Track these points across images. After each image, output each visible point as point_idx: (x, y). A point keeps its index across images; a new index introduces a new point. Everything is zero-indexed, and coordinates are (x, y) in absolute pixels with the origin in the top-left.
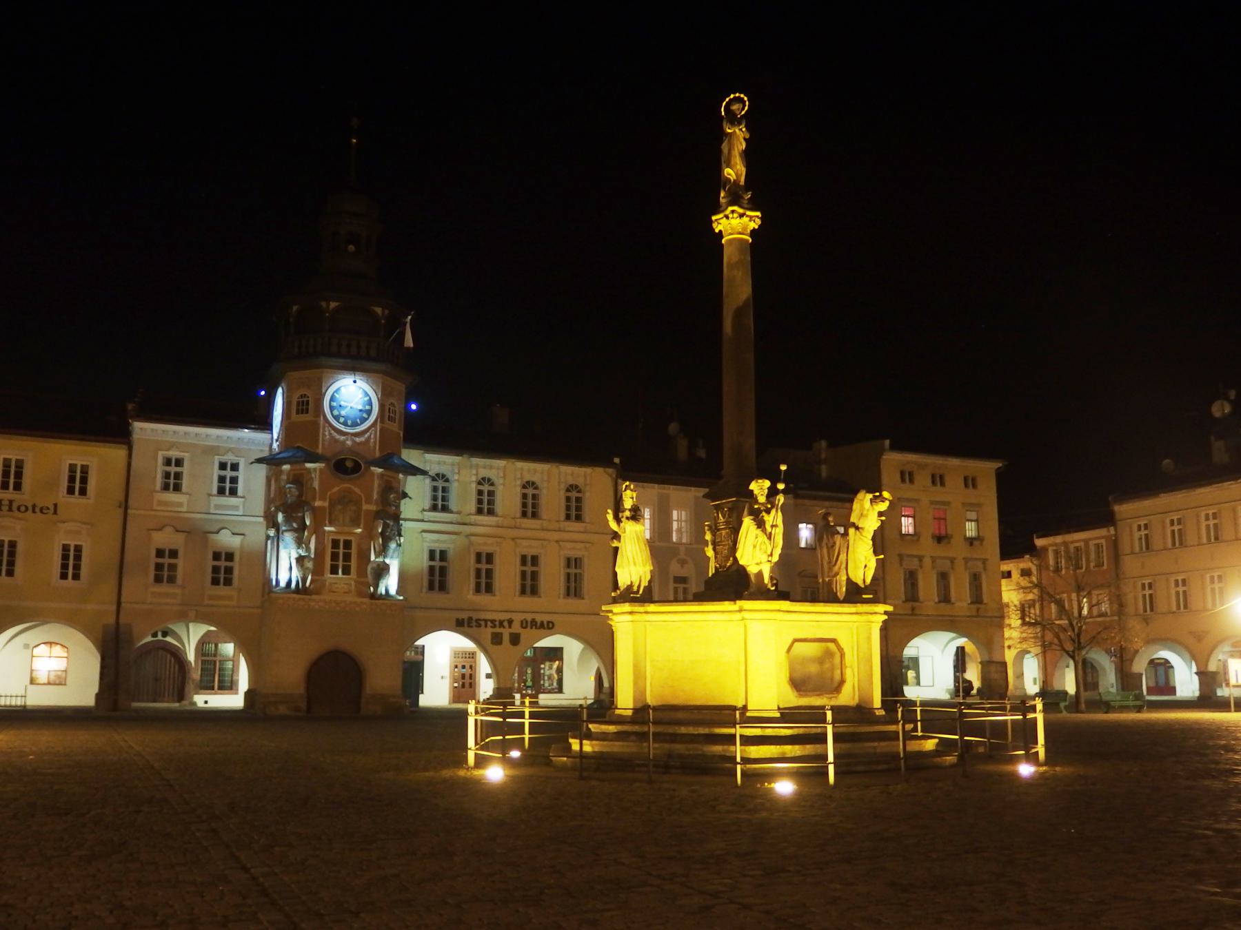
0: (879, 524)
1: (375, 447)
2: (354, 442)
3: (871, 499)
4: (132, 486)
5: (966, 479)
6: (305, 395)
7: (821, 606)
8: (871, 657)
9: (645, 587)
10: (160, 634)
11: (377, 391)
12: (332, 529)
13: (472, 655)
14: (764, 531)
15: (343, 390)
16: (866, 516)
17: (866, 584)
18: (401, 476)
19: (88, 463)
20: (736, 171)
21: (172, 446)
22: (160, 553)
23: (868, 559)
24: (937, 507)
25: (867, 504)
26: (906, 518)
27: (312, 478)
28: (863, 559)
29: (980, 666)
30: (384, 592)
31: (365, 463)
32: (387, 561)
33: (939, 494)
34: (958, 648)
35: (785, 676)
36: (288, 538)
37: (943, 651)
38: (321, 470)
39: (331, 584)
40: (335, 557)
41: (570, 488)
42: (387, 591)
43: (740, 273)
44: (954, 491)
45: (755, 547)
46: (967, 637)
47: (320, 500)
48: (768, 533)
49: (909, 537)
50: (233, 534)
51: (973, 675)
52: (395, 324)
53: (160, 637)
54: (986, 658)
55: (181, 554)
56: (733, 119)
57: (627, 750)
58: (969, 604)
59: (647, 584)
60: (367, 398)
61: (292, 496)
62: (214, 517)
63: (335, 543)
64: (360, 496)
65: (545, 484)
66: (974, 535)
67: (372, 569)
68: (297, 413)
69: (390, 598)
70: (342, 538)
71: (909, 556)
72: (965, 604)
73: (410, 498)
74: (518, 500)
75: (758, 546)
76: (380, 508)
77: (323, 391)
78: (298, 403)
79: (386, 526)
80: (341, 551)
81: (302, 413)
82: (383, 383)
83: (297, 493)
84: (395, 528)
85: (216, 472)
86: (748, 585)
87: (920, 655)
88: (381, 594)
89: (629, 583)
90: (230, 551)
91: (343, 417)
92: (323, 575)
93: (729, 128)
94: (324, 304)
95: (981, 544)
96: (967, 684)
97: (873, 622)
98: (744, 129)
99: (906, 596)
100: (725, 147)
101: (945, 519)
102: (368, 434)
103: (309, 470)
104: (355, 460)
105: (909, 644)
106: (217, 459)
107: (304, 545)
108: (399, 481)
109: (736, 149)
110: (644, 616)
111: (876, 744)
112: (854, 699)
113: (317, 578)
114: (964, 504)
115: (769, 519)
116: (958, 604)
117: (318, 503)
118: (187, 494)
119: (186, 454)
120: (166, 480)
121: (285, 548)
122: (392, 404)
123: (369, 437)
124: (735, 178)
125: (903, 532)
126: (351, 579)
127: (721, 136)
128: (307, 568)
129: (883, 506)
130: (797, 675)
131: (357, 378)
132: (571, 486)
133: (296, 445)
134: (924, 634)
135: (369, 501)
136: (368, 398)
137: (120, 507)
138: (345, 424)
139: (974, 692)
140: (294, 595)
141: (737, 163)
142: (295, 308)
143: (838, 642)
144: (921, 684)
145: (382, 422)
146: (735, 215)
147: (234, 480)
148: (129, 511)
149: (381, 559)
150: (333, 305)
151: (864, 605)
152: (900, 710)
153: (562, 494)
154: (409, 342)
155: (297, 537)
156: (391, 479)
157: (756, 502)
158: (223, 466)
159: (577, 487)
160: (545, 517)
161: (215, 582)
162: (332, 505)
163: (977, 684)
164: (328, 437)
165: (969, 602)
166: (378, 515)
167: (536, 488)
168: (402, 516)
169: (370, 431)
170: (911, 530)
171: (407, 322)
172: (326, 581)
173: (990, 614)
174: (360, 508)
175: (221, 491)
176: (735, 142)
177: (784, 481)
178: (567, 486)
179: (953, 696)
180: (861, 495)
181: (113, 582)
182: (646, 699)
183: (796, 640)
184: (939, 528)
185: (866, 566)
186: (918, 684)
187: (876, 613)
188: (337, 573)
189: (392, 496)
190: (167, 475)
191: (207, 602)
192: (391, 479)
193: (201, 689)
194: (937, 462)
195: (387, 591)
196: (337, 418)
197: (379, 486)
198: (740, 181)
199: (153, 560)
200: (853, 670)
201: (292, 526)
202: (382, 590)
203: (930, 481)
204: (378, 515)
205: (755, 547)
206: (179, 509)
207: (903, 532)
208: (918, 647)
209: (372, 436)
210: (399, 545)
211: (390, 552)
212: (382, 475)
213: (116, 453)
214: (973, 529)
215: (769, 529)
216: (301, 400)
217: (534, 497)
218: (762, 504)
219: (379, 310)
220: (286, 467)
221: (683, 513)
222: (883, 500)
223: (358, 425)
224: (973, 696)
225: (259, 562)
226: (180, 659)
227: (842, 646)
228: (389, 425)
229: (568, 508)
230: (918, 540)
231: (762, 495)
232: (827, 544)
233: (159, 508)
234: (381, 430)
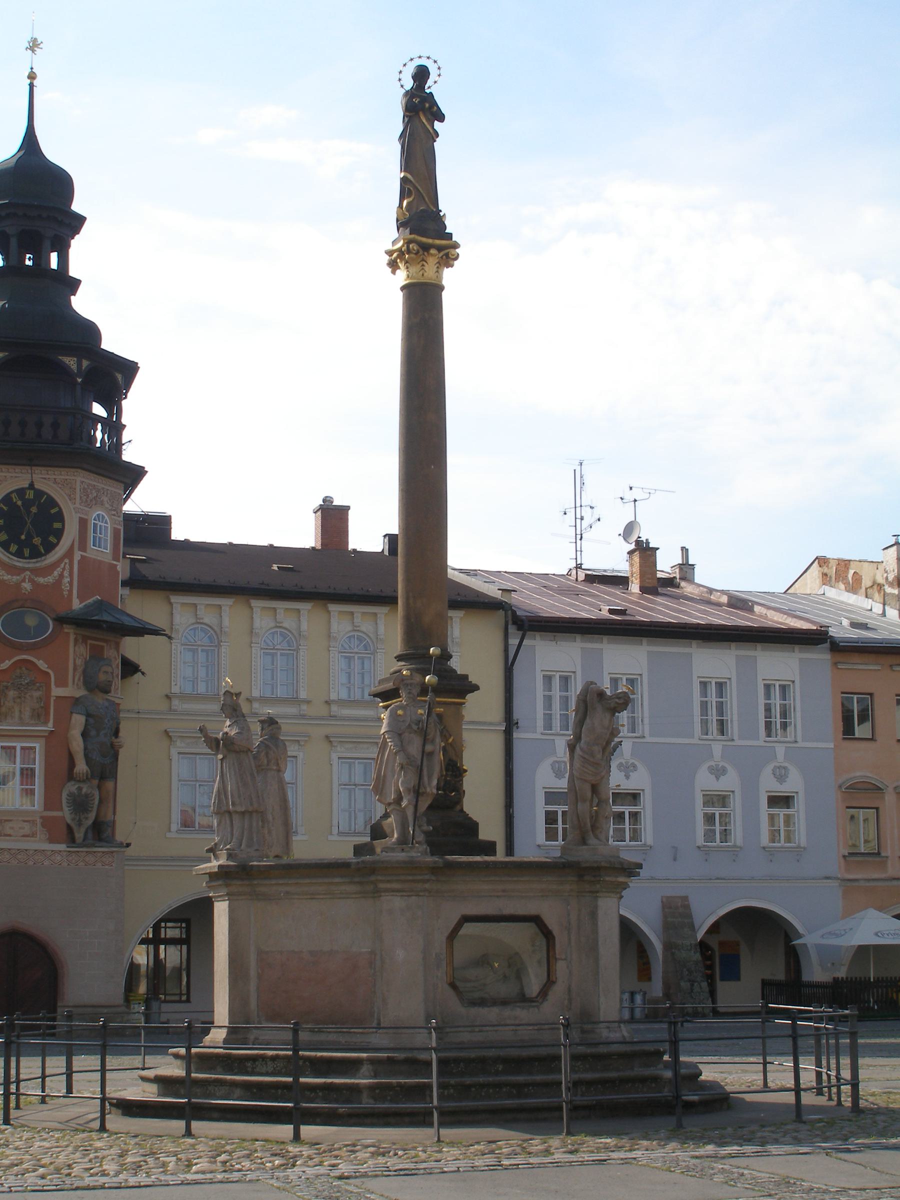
1: (70, 591)
13: (613, 805)
31: (55, 620)
64: (47, 674)
66: (792, 1058)
73: (143, 673)
123: (61, 576)
169: (62, 565)
208: (877, 809)
209: (66, 574)
226: (306, 864)
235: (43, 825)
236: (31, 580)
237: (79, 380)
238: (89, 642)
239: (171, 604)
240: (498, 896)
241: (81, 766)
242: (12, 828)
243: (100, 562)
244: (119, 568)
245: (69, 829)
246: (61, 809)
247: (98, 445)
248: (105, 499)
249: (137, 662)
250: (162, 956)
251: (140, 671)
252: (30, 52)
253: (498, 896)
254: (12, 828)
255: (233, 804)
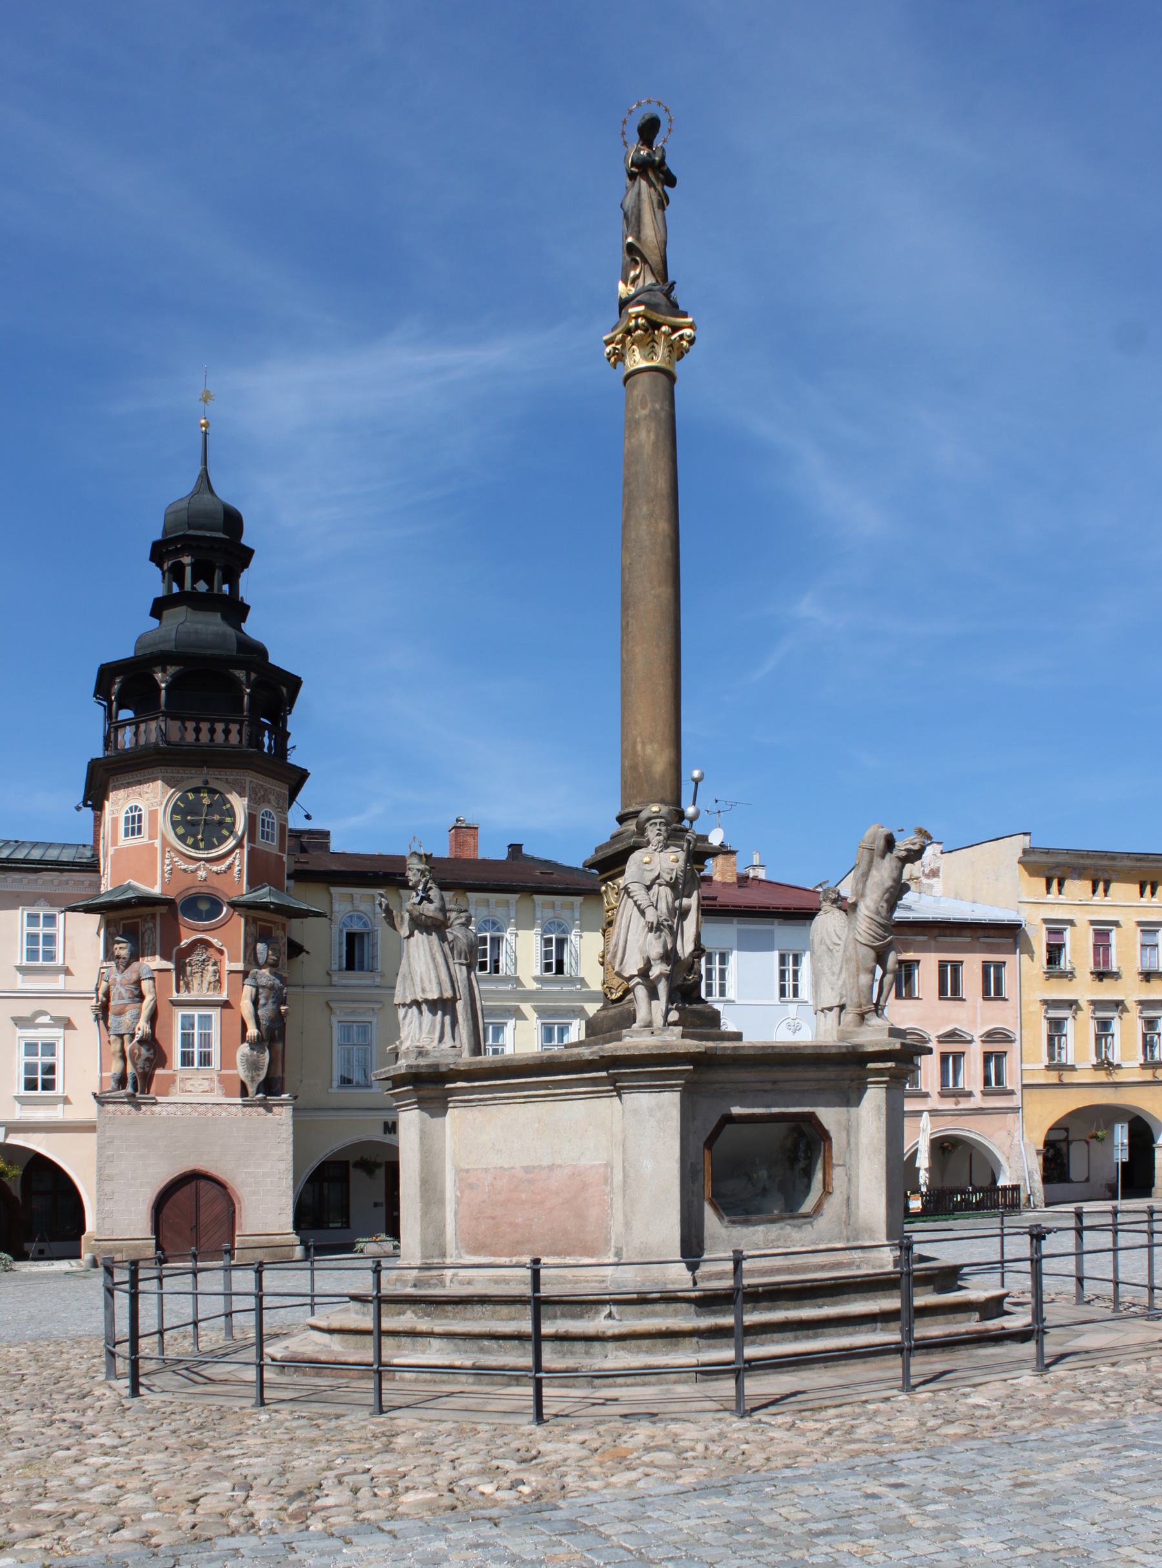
68: (126, 835)
73: (308, 953)
78: (127, 819)
81: (133, 834)
145: (252, 839)
151: (55, 1262)
209: (237, 862)
216: (130, 815)
234: (249, 853)
235: (220, 1081)
236: (205, 869)
237: (248, 690)
238: (259, 923)
239: (331, 895)
240: (766, 1091)
241: (252, 1031)
242: (192, 1085)
243: (268, 853)
244: (285, 859)
245: (243, 1085)
246: (235, 1068)
247: (266, 750)
248: (272, 798)
249: (301, 943)
250: (326, 1192)
251: (305, 951)
252: (202, 403)
253: (766, 1091)
254: (192, 1085)
255: (423, 991)
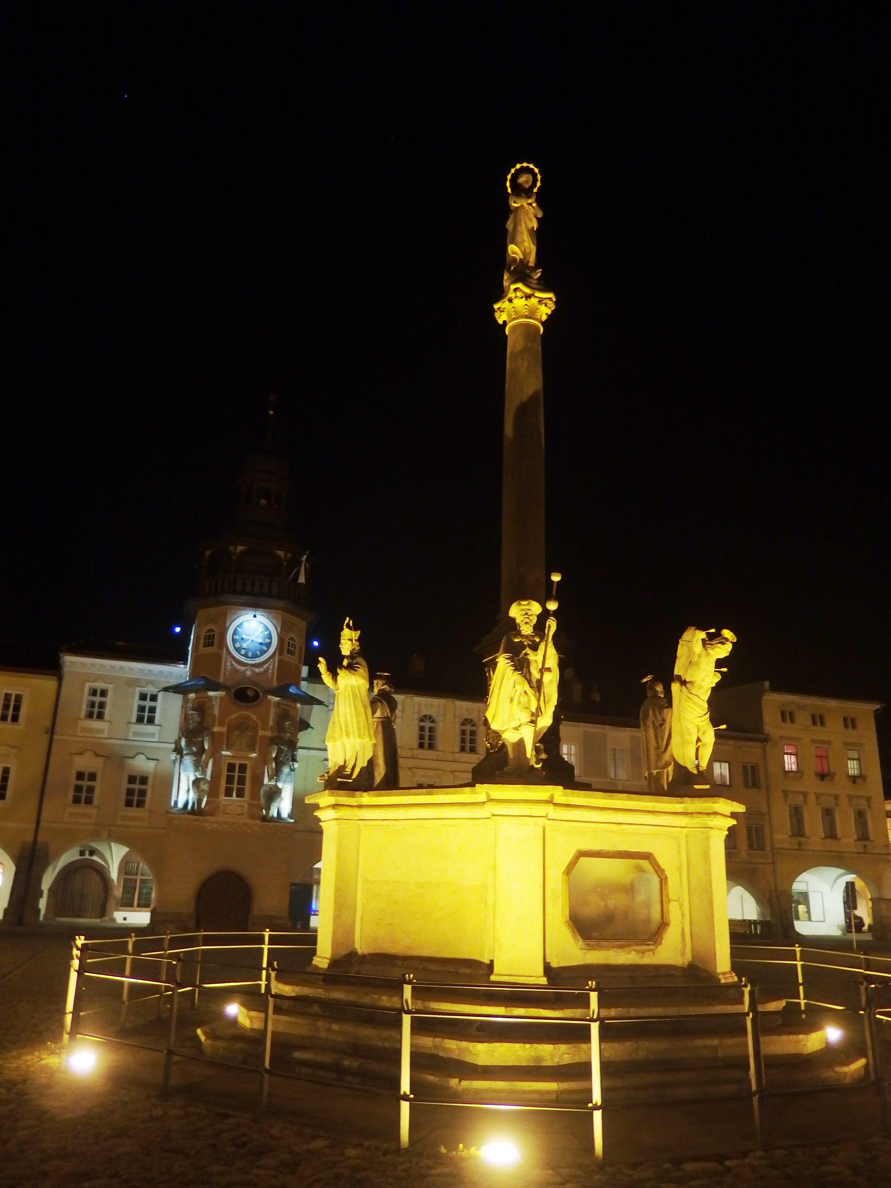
0: (717, 678)
1: (273, 677)
2: (253, 672)
3: (703, 640)
4: (60, 715)
5: (845, 719)
6: (212, 629)
7: (622, 799)
8: (711, 886)
9: (362, 769)
10: (87, 853)
11: (277, 626)
12: (228, 753)
14: (527, 677)
15: (245, 625)
16: (697, 664)
17: (701, 769)
18: (299, 705)
19: (21, 693)
20: (523, 250)
21: (98, 678)
22: (80, 776)
23: (702, 730)
24: (820, 745)
25: (698, 647)
26: (789, 756)
27: (213, 706)
28: (694, 730)
29: (870, 903)
30: (275, 815)
32: (280, 785)
33: (820, 733)
34: (847, 883)
35: (559, 913)
36: (188, 760)
37: (832, 888)
38: (221, 698)
39: (225, 806)
40: (229, 780)
41: (472, 723)
42: (279, 813)
43: (526, 364)
44: (834, 731)
45: (512, 700)
46: (855, 874)
47: (219, 725)
48: (534, 681)
49: (792, 774)
50: (148, 759)
51: (864, 911)
52: (295, 563)
53: (87, 856)
54: (876, 896)
55: (99, 777)
56: (519, 191)
57: (297, 1031)
58: (855, 841)
59: (365, 765)
60: (267, 632)
61: (194, 722)
62: (132, 743)
63: (231, 767)
65: (441, 719)
67: (265, 792)
69: (281, 821)
70: (237, 762)
71: (793, 792)
72: (851, 840)
74: (416, 733)
75: (515, 701)
76: (276, 734)
77: (227, 625)
79: (280, 752)
80: (236, 774)
81: (208, 646)
82: (283, 618)
83: (198, 720)
84: (289, 754)
85: (136, 702)
86: (506, 763)
87: (809, 890)
88: (273, 817)
89: (342, 764)
90: (145, 775)
91: (243, 649)
92: (218, 797)
93: (514, 202)
94: (232, 548)
95: (865, 782)
96: (859, 921)
97: (711, 828)
98: (534, 205)
99: (792, 832)
100: (509, 225)
101: (827, 757)
102: (267, 665)
103: (210, 698)
104: (255, 690)
105: (798, 879)
106: (138, 691)
107: (200, 768)
108: (296, 710)
109: (523, 225)
110: (356, 810)
111: (716, 1042)
112: (683, 954)
113: (212, 799)
114: (845, 744)
115: (535, 658)
116: (844, 841)
117: (216, 729)
118: (109, 721)
119: (110, 685)
120: (91, 709)
121: (185, 771)
122: (291, 639)
123: (268, 668)
124: (522, 257)
125: (787, 769)
126: (244, 801)
127: (506, 211)
128: (203, 790)
129: (723, 651)
130: (594, 907)
131: (258, 614)
132: (466, 720)
133: (202, 675)
134: (809, 870)
135: (264, 729)
136: (268, 632)
137: (47, 732)
138: (246, 655)
139: (866, 928)
140: (191, 816)
141: (524, 241)
142: (208, 553)
143: (655, 860)
144: (812, 919)
145: (281, 654)
146: (519, 294)
147: (152, 710)
148: (56, 737)
149: (273, 783)
150: (240, 548)
151: (695, 800)
152: (747, 990)
153: (458, 727)
154: (302, 579)
155: (195, 761)
156: (288, 708)
157: (519, 634)
158: (143, 697)
159: (471, 721)
160: (440, 748)
161: (129, 804)
162: (230, 730)
163: (867, 921)
164: (229, 667)
165: (856, 838)
166: (273, 741)
167: (433, 722)
168: (299, 745)
169: (269, 663)
170: (794, 768)
171: (302, 562)
172: (219, 803)
173: (877, 851)
174: (256, 734)
175: (140, 720)
176: (522, 217)
177: (556, 598)
178: (463, 720)
179: (845, 932)
180: (687, 635)
181: (33, 804)
182: (354, 943)
183: (582, 854)
184: (822, 766)
185: (698, 740)
186: (810, 919)
187: (716, 813)
188: (231, 796)
189: (287, 723)
190: (92, 705)
191: (119, 822)
192: (288, 708)
193: (121, 906)
194: (816, 703)
195: (279, 813)
196: (238, 650)
197: (275, 713)
198: (529, 262)
199: (74, 782)
200: (681, 906)
201: (192, 750)
202: (274, 812)
203: (810, 721)
204: (273, 741)
205: (512, 700)
206: (100, 736)
207: (787, 769)
208: (807, 882)
210: (292, 770)
211: (283, 776)
212: (279, 704)
213: (47, 684)
214: (855, 767)
215: (536, 675)
217: (431, 730)
218: (526, 637)
219: (281, 554)
220: (192, 696)
221: (573, 747)
222: (724, 641)
223: (258, 656)
224: (864, 932)
225: (166, 783)
227: (663, 867)
228: (287, 657)
229: (463, 741)
230: (801, 777)
231: (526, 623)
232: (653, 723)
233: (81, 734)
242: (230, 810)
